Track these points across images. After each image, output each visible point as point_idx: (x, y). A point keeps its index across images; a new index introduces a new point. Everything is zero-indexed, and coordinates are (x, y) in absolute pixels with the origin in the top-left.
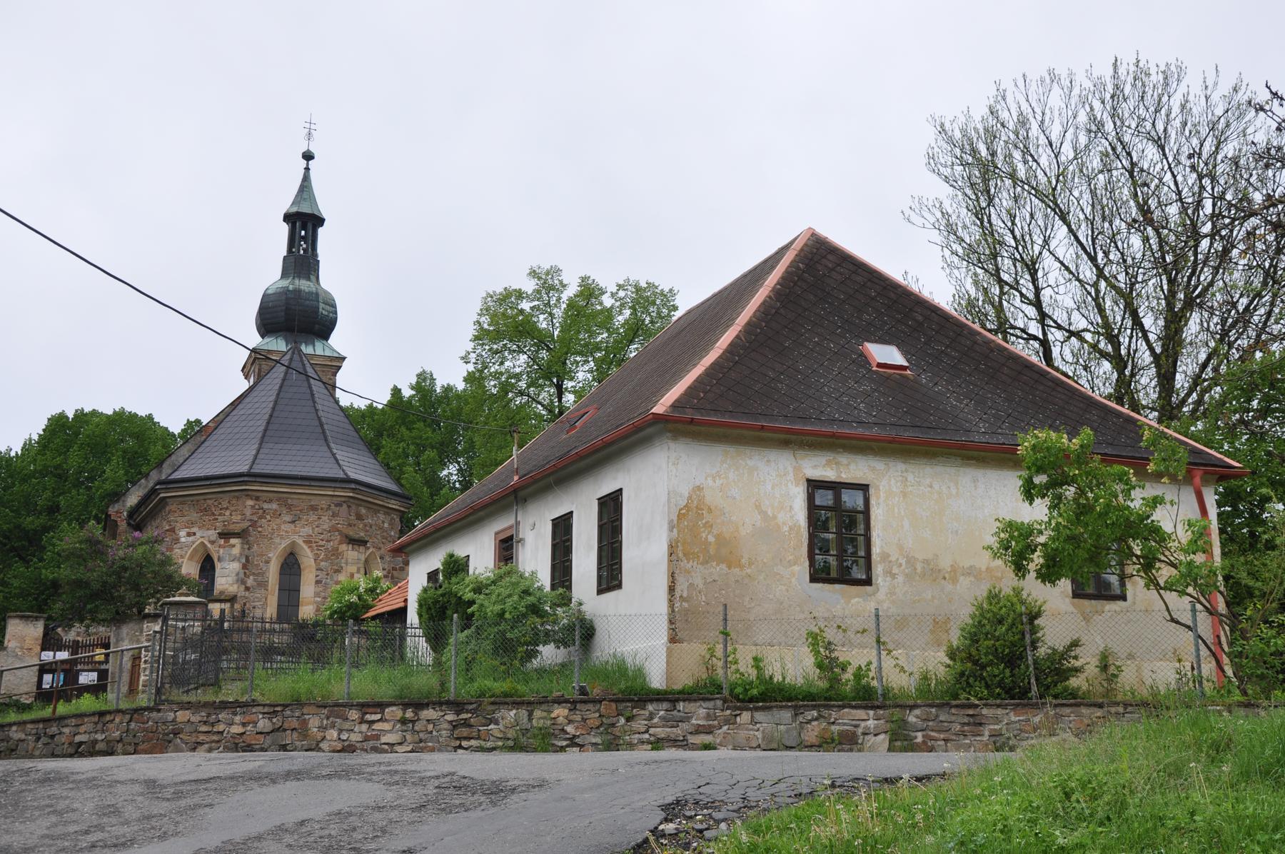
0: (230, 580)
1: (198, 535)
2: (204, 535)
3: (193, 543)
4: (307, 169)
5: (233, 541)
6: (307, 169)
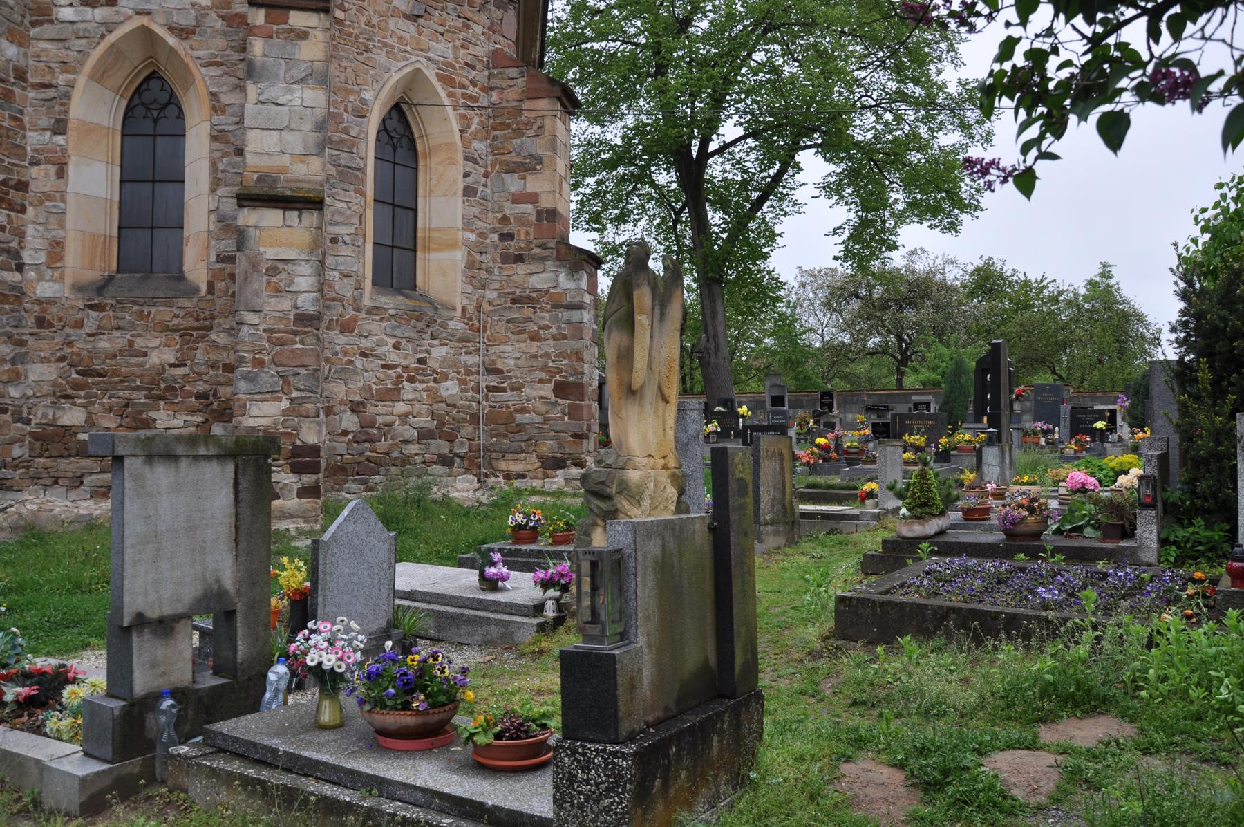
0: (295, 141)
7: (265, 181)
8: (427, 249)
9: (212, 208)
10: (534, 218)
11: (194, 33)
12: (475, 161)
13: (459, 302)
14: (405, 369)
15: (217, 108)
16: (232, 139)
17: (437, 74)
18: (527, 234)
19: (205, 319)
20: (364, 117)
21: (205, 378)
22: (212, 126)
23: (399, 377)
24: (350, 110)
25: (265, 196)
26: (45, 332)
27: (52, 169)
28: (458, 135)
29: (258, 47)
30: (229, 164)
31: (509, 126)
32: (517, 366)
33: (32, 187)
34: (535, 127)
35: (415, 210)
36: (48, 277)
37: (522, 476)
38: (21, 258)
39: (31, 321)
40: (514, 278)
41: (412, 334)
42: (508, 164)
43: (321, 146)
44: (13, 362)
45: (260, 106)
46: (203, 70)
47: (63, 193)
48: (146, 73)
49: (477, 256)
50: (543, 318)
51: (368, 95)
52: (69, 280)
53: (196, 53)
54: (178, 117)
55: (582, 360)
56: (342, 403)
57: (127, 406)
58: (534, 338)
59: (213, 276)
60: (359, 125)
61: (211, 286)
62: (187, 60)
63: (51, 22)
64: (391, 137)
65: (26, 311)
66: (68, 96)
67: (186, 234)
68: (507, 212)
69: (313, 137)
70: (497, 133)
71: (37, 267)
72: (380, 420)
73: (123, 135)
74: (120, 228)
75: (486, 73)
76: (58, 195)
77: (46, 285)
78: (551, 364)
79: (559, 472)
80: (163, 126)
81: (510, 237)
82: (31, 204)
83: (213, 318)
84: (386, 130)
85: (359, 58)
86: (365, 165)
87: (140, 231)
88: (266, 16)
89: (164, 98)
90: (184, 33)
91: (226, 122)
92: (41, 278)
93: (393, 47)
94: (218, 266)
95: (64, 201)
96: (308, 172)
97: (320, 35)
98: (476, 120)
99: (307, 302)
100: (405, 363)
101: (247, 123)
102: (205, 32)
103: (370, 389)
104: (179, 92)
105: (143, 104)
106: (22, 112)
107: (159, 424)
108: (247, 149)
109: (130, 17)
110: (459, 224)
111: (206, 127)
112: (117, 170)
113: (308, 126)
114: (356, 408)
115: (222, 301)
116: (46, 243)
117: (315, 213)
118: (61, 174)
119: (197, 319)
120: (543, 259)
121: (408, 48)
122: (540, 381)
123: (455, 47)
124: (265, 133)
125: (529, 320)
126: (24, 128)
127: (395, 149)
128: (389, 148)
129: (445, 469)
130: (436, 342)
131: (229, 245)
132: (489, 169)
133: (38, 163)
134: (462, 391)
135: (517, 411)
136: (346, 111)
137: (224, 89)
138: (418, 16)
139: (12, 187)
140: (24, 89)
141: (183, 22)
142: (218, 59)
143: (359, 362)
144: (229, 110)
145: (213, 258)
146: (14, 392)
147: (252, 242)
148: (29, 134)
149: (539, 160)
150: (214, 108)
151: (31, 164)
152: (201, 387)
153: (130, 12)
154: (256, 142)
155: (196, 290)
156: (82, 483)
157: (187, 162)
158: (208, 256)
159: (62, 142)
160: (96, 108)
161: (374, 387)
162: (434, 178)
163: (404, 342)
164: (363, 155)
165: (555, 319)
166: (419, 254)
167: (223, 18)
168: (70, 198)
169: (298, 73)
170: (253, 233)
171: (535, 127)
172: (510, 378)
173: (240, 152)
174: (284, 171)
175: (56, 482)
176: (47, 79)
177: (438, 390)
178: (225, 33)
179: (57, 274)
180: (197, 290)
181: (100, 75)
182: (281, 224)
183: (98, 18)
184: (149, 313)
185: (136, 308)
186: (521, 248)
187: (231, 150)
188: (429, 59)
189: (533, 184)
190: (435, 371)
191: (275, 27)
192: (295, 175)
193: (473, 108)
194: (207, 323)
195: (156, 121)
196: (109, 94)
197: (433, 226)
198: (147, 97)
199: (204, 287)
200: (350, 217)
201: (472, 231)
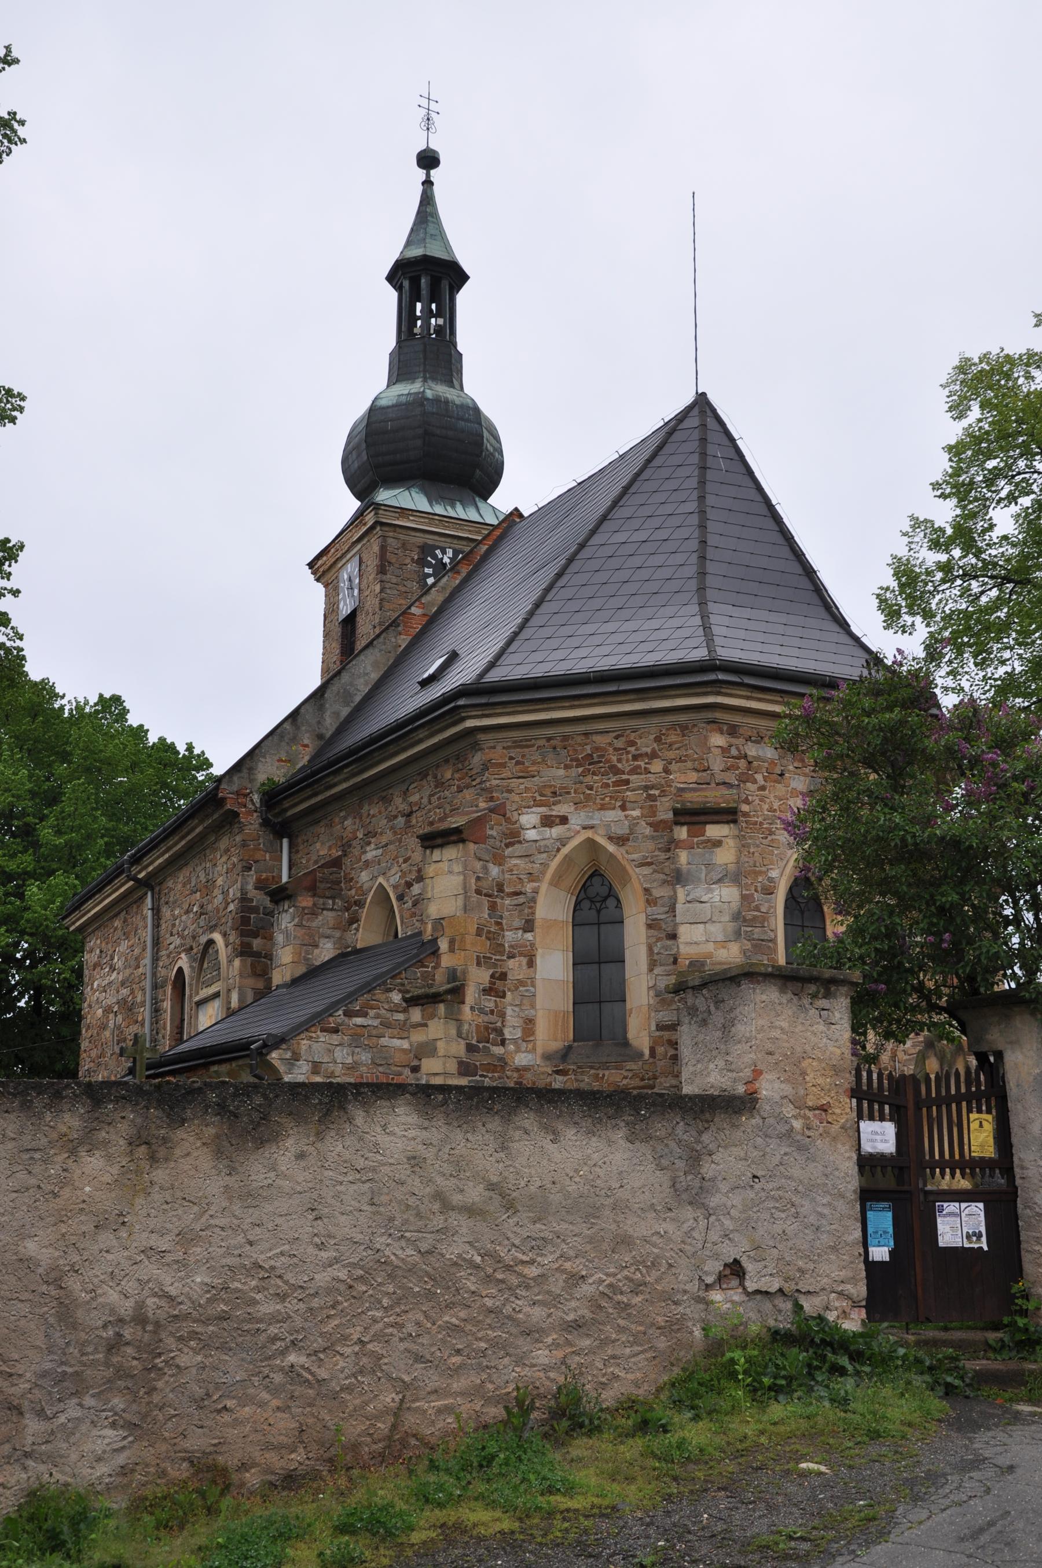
0: (717, 931)
1: (577, 820)
2: (590, 824)
3: (563, 842)
4: (428, 183)
5: (713, 831)
6: (428, 183)
9: (651, 985)
11: (628, 840)
15: (651, 901)
16: (664, 927)
19: (649, 1079)
20: (772, 893)
22: (647, 916)
24: (759, 889)
27: (524, 961)
29: (683, 857)
30: (663, 947)
33: (510, 976)
36: (523, 1049)
43: (738, 934)
45: (688, 905)
46: (637, 870)
47: (533, 980)
48: (590, 873)
51: (774, 874)
52: (539, 1051)
59: (654, 1042)
60: (768, 901)
61: (652, 1050)
62: (624, 863)
63: (520, 842)
65: (508, 1078)
66: (534, 900)
67: (629, 1005)
69: (731, 927)
71: (515, 1041)
73: (573, 926)
74: (574, 1004)
76: (529, 981)
77: (523, 1055)
82: (509, 990)
83: (655, 1078)
84: (793, 897)
85: (765, 841)
86: (776, 936)
87: (590, 1006)
89: (604, 891)
90: (620, 840)
91: (659, 912)
92: (518, 1050)
94: (658, 1033)
95: (534, 986)
97: (731, 842)
101: (678, 919)
104: (617, 887)
105: (588, 898)
109: (579, 832)
111: (642, 919)
112: (571, 954)
113: (726, 918)
115: (662, 1063)
116: (521, 1021)
118: (531, 964)
119: (642, 1080)
124: (693, 926)
126: (503, 930)
127: (802, 912)
136: (756, 891)
137: (655, 884)
140: (502, 898)
141: (620, 832)
142: (649, 860)
144: (660, 902)
145: (653, 1028)
150: (648, 901)
151: (509, 958)
153: (578, 828)
154: (687, 933)
158: (649, 1025)
160: (554, 907)
164: (774, 928)
168: (539, 983)
173: (674, 936)
174: (710, 955)
176: (518, 888)
178: (653, 838)
179: (530, 1046)
180: (642, 1055)
181: (556, 882)
183: (554, 836)
184: (604, 1075)
185: (592, 1071)
187: (663, 935)
191: (696, 840)
192: (719, 959)
194: (651, 1082)
195: (599, 911)
196: (563, 894)
198: (592, 892)
199: (647, 1052)
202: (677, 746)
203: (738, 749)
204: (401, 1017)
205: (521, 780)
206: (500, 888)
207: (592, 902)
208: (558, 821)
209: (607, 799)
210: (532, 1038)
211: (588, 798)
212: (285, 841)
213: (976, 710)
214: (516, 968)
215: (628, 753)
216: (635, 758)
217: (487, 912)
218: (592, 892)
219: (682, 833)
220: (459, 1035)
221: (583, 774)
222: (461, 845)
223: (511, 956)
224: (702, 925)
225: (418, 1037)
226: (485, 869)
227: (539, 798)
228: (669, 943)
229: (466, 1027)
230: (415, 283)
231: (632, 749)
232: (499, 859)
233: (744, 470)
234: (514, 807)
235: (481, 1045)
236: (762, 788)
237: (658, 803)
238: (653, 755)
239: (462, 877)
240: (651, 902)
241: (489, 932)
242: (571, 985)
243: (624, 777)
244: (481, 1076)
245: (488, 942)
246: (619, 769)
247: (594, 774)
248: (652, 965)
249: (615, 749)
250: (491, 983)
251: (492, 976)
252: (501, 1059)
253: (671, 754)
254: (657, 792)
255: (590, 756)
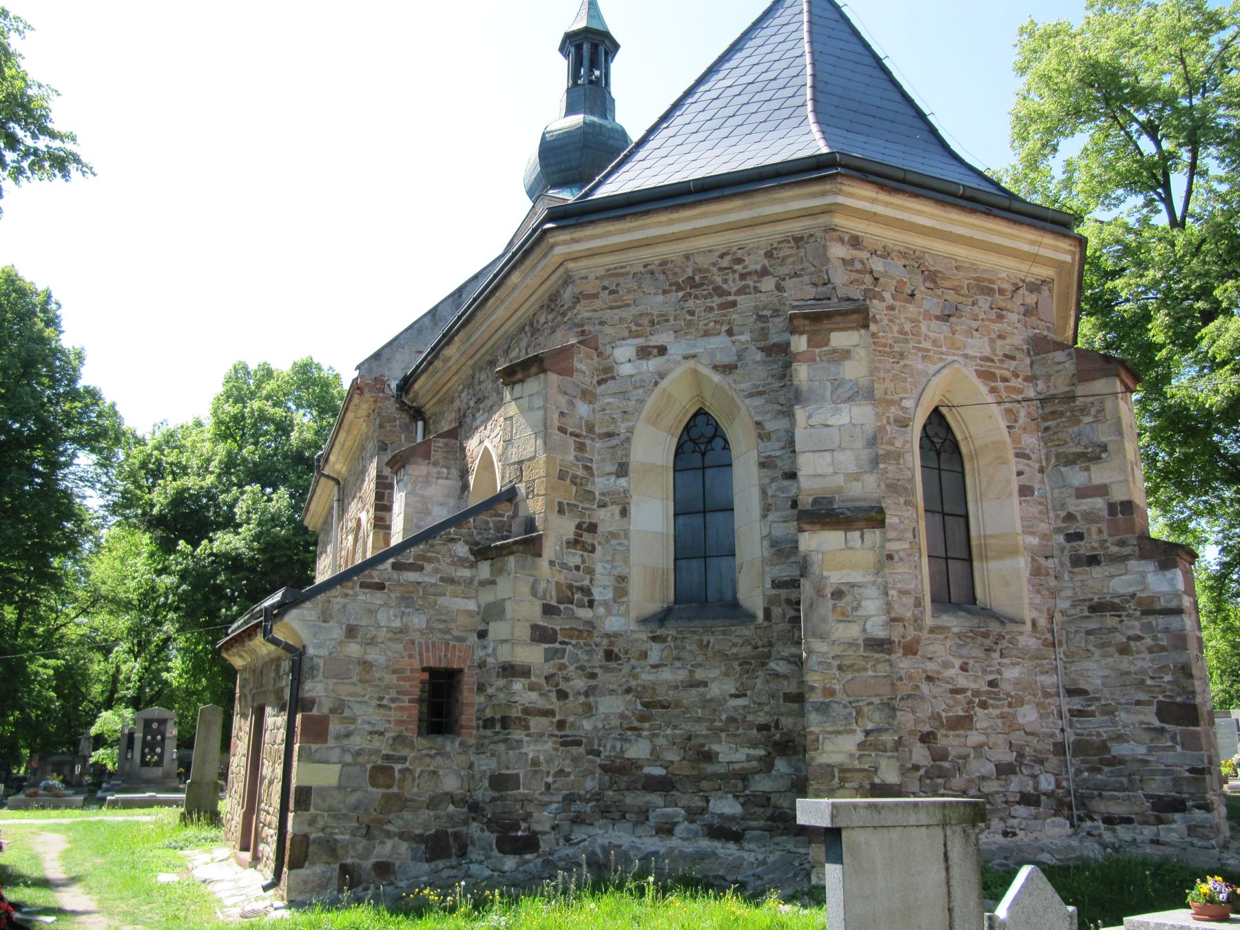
0: (848, 461)
5: (839, 339)
7: (820, 503)
8: (984, 557)
9: (764, 533)
10: (1105, 513)
12: (1027, 457)
13: (1028, 615)
14: (976, 693)
17: (977, 371)
18: (1100, 531)
21: (767, 708)
23: (970, 702)
25: (824, 514)
26: (613, 665)
27: (616, 509)
28: (1005, 431)
29: (802, 373)
31: (1062, 414)
32: (1104, 685)
33: (600, 529)
34: (1093, 411)
35: (966, 517)
37: (1128, 821)
38: (592, 594)
39: (601, 654)
40: (1090, 583)
41: (979, 653)
42: (1066, 455)
43: (875, 462)
44: (587, 694)
46: (747, 401)
47: (627, 534)
49: (1042, 561)
50: (1132, 627)
51: (907, 403)
52: (633, 614)
53: (739, 387)
54: (724, 448)
55: (1191, 676)
56: (911, 733)
57: (689, 738)
58: (1124, 650)
61: (768, 613)
63: (613, 378)
64: (933, 443)
66: (628, 440)
68: (1072, 509)
69: (865, 454)
70: (1049, 423)
72: (953, 753)
73: (675, 471)
74: (676, 559)
75: (1028, 361)
77: (614, 619)
78: (1149, 682)
79: (1177, 816)
80: (709, 460)
81: (1079, 536)
83: (771, 644)
84: (927, 436)
86: (913, 476)
88: (809, 342)
89: (710, 431)
91: (773, 448)
92: (609, 612)
93: (928, 350)
94: (774, 592)
96: (866, 488)
97: (861, 352)
98: (1023, 413)
99: (877, 628)
100: (973, 686)
102: (747, 365)
103: (940, 717)
104: (724, 425)
105: (691, 440)
106: (591, 460)
107: (722, 758)
108: (800, 473)
110: (1019, 529)
112: (672, 503)
113: (860, 444)
114: (927, 738)
116: (612, 579)
117: (878, 531)
118: (624, 512)
120: (1125, 559)
121: (944, 349)
122: (1138, 703)
123: (992, 341)
125: (1114, 630)
126: (593, 475)
128: (933, 454)
129: (1032, 810)
130: (1006, 661)
131: (785, 571)
132: (1044, 464)
133: (604, 505)
134: (1041, 716)
135: (1111, 739)
137: (768, 416)
138: (949, 316)
139: (585, 530)
140: (593, 440)
142: (761, 389)
143: (925, 688)
144: (774, 437)
145: (768, 585)
146: (587, 725)
147: (815, 566)
148: (597, 480)
149: (1104, 448)
150: (760, 436)
152: (762, 719)
153: (679, 358)
155: (752, 617)
156: (647, 819)
157: (735, 490)
158: (763, 581)
159: (625, 484)
161: (944, 714)
162: (984, 480)
163: (971, 662)
165: (1148, 628)
166: (976, 564)
167: (762, 349)
168: (632, 535)
169: (843, 392)
170: (816, 558)
171: (1093, 411)
172: (1098, 699)
173: (792, 476)
174: (839, 490)
175: (623, 817)
176: (611, 428)
177: (1014, 716)
178: (764, 362)
179: (623, 608)
182: (843, 546)
185: (696, 637)
186: (1093, 548)
187: (779, 474)
188: (966, 356)
189: (1099, 475)
190: (1008, 695)
191: (817, 350)
193: (1019, 402)
194: (766, 650)
195: (703, 454)
197: (988, 532)
198: (694, 434)
200: (903, 531)
201: (1033, 534)
202: (791, 260)
203: (862, 262)
204: (466, 573)
205: (616, 311)
206: (590, 428)
207: (696, 444)
208: (655, 351)
209: (712, 324)
210: (625, 599)
211: (689, 324)
212: (420, 424)
213: (593, 895)
214: (607, 518)
215: (734, 272)
216: (743, 277)
217: (573, 453)
218: (694, 434)
219: (800, 343)
220: (534, 593)
221: (685, 299)
222: (542, 376)
223: (603, 505)
224: (827, 455)
225: (487, 597)
226: (571, 404)
227: (634, 328)
228: (786, 483)
229: (543, 585)
230: (579, 48)
231: (739, 267)
232: (587, 396)
233: (849, 30)
234: (608, 339)
235: (562, 607)
236: (891, 308)
237: (770, 325)
238: (764, 272)
239: (541, 413)
240: (764, 436)
241: (575, 476)
242: (672, 538)
243: (730, 298)
244: (561, 643)
245: (574, 488)
246: (724, 291)
247: (696, 297)
248: (766, 510)
249: (720, 269)
250: (576, 534)
251: (579, 526)
252: (590, 623)
253: (784, 270)
254: (768, 313)
255: (693, 278)
